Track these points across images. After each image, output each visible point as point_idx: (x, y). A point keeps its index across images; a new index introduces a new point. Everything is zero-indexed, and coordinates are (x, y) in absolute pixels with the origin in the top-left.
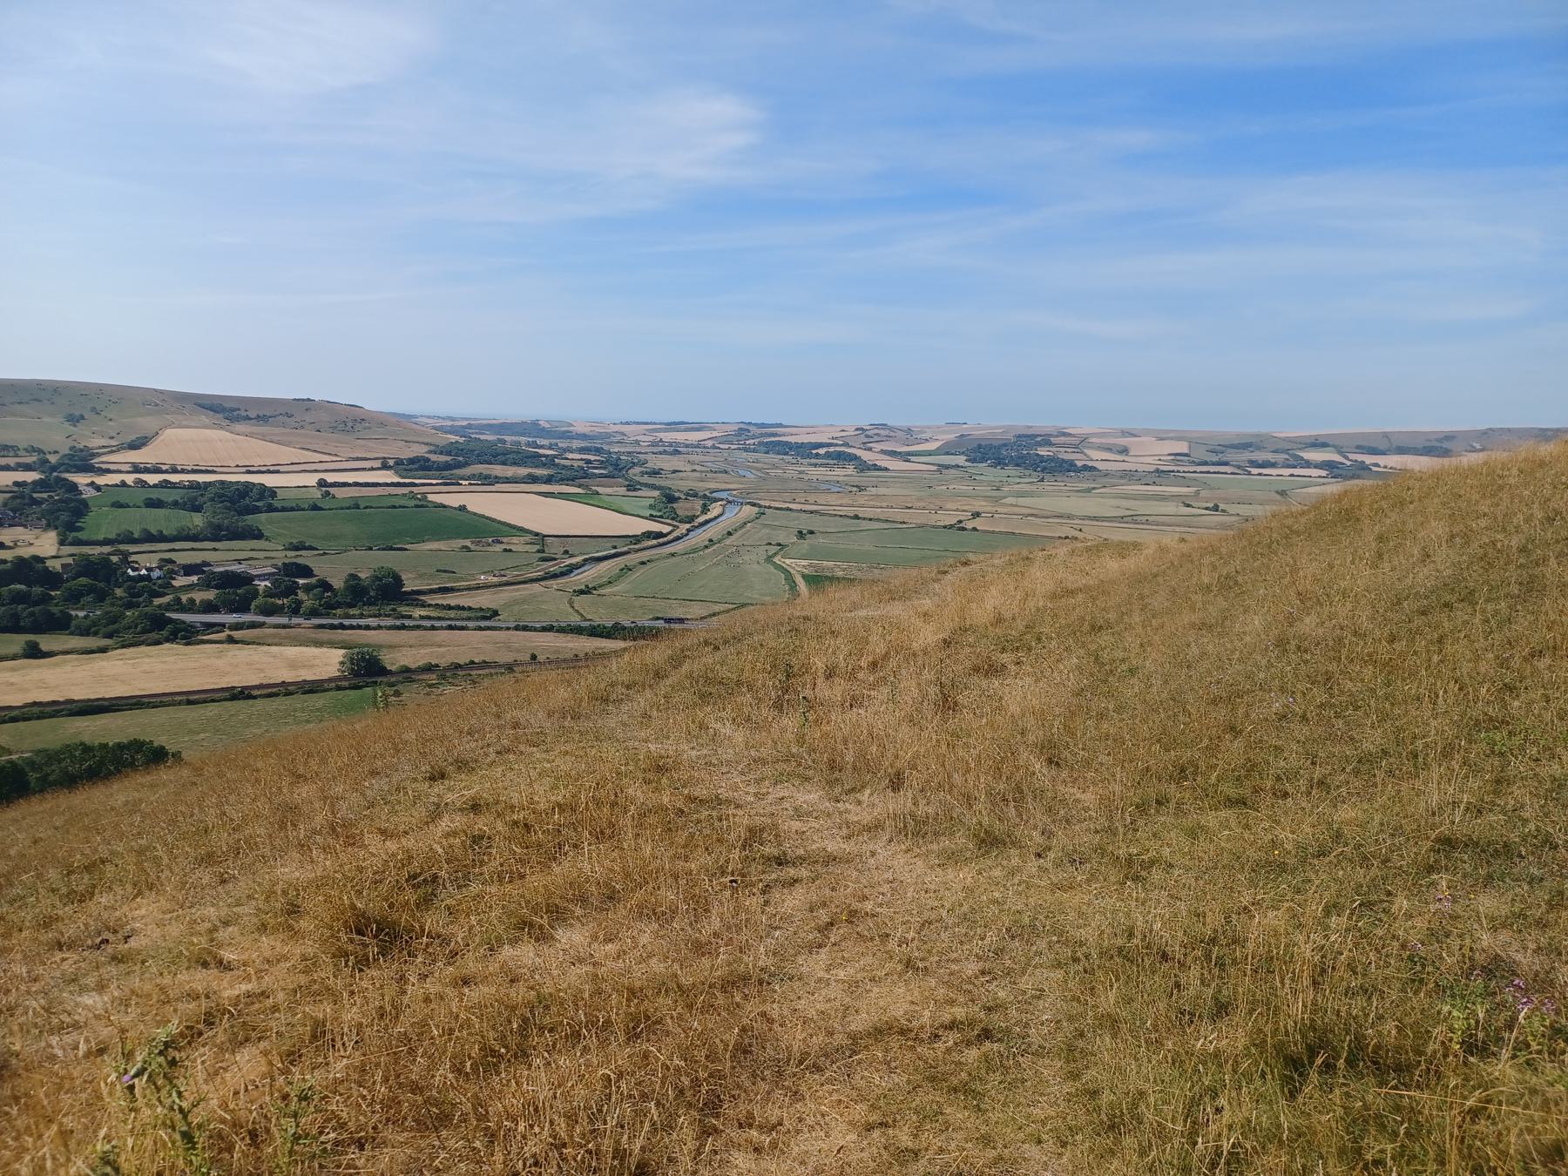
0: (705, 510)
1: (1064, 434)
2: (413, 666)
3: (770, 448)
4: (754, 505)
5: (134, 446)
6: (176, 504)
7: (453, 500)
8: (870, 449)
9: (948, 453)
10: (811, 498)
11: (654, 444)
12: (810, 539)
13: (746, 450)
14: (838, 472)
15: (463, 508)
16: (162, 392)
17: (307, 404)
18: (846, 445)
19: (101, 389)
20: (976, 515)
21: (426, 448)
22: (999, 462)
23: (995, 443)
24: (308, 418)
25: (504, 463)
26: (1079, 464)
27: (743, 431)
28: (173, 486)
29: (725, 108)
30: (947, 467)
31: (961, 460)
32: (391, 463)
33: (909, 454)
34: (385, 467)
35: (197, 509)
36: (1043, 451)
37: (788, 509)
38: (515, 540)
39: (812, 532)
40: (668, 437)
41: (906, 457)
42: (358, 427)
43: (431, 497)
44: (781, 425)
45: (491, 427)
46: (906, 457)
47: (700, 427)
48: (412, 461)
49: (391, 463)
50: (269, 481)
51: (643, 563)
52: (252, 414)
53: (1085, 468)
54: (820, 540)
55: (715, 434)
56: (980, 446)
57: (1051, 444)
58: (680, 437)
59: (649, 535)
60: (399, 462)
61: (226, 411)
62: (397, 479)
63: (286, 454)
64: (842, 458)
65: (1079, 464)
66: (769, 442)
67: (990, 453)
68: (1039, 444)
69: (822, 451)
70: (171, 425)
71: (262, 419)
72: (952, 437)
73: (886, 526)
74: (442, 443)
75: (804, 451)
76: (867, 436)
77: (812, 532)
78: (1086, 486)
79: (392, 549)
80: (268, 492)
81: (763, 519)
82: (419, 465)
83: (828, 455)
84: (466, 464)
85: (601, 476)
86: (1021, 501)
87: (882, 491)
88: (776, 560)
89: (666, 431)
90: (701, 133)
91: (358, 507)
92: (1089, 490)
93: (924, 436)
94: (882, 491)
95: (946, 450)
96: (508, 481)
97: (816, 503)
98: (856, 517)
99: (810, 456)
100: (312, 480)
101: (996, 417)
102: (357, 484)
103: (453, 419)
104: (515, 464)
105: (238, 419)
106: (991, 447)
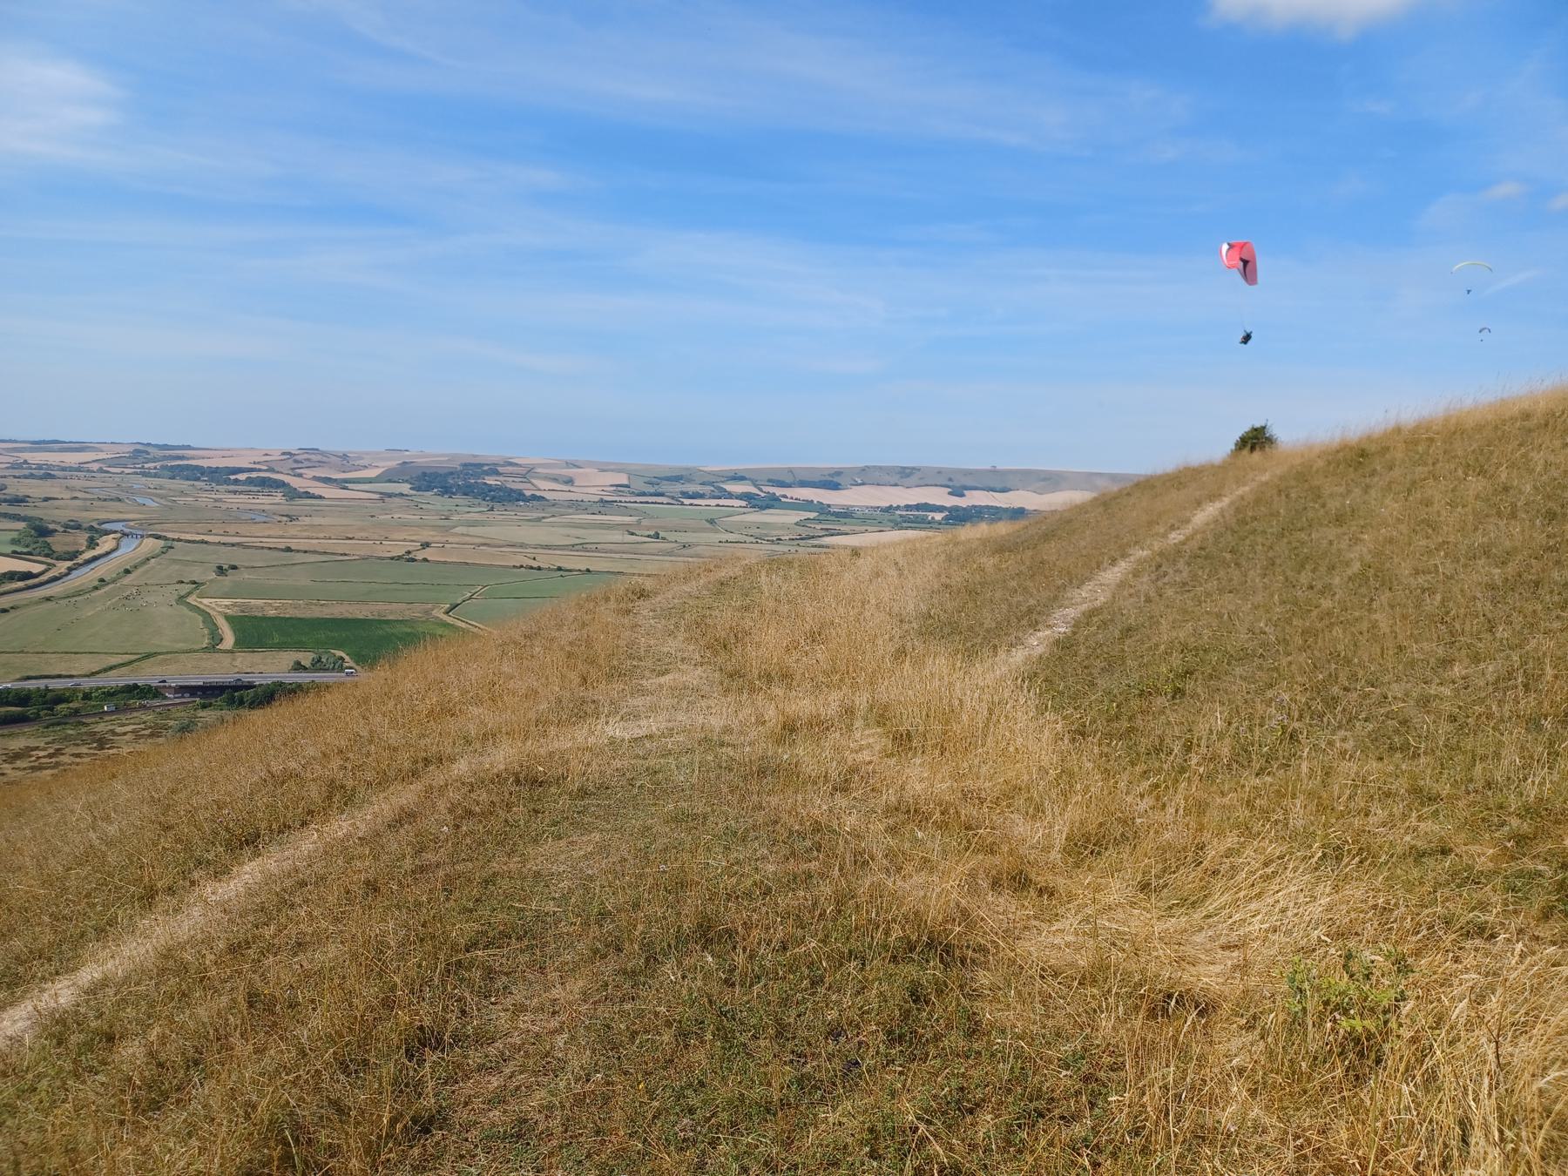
1: (511, 464)
3: (176, 472)
10: (232, 529)
13: (144, 474)
18: (271, 470)
26: (528, 493)
30: (390, 495)
31: (405, 488)
33: (346, 481)
36: (491, 481)
39: (234, 568)
44: (189, 448)
47: (81, 448)
57: (498, 473)
58: (53, 458)
64: (264, 483)
66: (181, 468)
67: (435, 480)
68: (487, 473)
69: (242, 477)
73: (324, 558)
76: (296, 460)
77: (234, 568)
83: (250, 481)
86: (472, 530)
87: (317, 520)
93: (361, 462)
95: (388, 477)
97: (226, 533)
99: (227, 482)
101: (442, 446)
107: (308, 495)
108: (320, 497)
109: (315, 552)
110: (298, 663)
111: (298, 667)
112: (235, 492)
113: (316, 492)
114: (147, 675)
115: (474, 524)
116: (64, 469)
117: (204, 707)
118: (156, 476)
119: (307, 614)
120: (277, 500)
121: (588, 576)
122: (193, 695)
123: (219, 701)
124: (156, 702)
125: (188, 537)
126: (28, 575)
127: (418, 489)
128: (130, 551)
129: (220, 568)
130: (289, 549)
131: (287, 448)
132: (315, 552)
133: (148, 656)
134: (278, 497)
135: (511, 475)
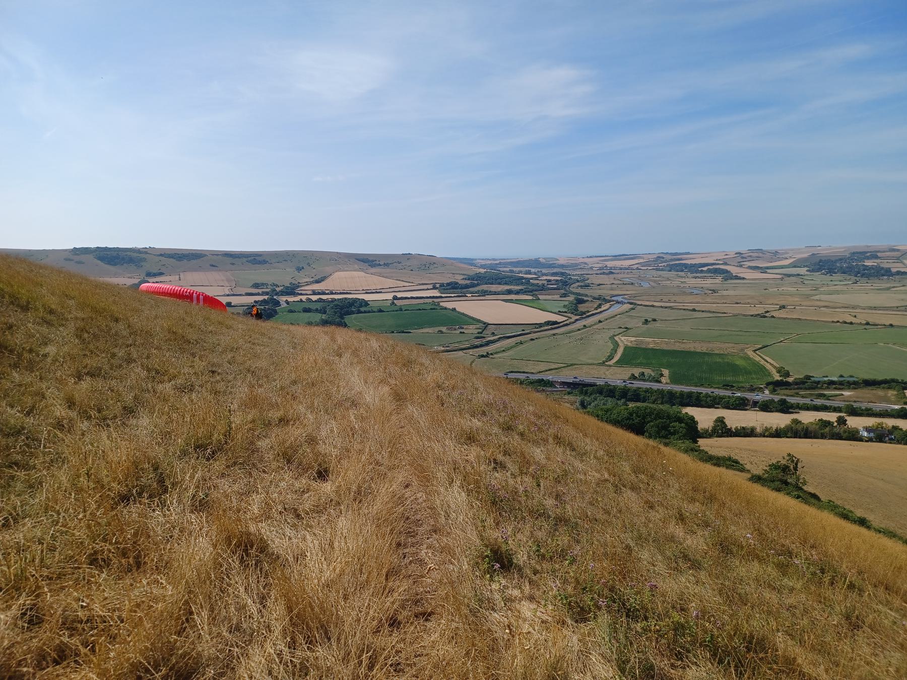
0: (600, 306)
1: (894, 250)
2: (817, 375)
3: (671, 268)
4: (631, 303)
5: (318, 282)
6: (317, 310)
7: (450, 305)
8: (741, 266)
9: (795, 267)
10: (665, 299)
11: (601, 269)
12: (651, 325)
13: (657, 270)
14: (709, 281)
15: (454, 309)
16: (340, 254)
17: (408, 256)
18: (725, 264)
19: (312, 253)
20: (783, 307)
21: (463, 277)
22: (831, 271)
23: (833, 259)
24: (408, 263)
25: (500, 284)
26: (894, 270)
27: (659, 258)
28: (323, 301)
29: (564, 73)
30: (789, 276)
31: (803, 271)
32: (438, 286)
33: (768, 268)
34: (434, 288)
35: (325, 313)
36: (868, 263)
37: (653, 306)
38: (471, 327)
39: (654, 320)
40: (610, 264)
41: (763, 270)
42: (431, 267)
43: (442, 304)
44: (688, 253)
45: (518, 263)
46: (763, 270)
47: (634, 257)
48: (448, 284)
49: (438, 286)
50: (367, 297)
51: (532, 340)
52: (382, 263)
53: (898, 273)
54: (657, 325)
55: (641, 261)
56: (821, 261)
57: (877, 257)
58: (618, 263)
59: (548, 323)
60: (442, 285)
61: (368, 262)
62: (439, 295)
63: (390, 283)
64: (717, 272)
65: (894, 270)
66: (678, 265)
67: (825, 265)
68: (868, 258)
69: (705, 269)
70: (340, 270)
71: (386, 265)
72: (806, 255)
73: (711, 315)
74: (471, 273)
75: (694, 269)
76: (741, 258)
77: (654, 320)
78: (888, 285)
79: (403, 332)
80: (366, 303)
81: (633, 313)
82: (453, 287)
83: (709, 271)
84: (478, 285)
85: (554, 289)
86: (833, 297)
87: (725, 293)
88: (616, 338)
89: (612, 260)
90: (552, 91)
91: (401, 310)
92: (888, 289)
93: (786, 256)
94: (725, 293)
95: (794, 265)
96: (495, 293)
97: (675, 302)
98: (694, 310)
99: (697, 272)
100: (390, 296)
101: (836, 241)
102: (412, 298)
103: (494, 260)
104: (506, 284)
105: (373, 266)
106: (829, 261)
107: (737, 278)
108: (744, 278)
109: (709, 312)
110: (633, 375)
111: (633, 377)
112: (696, 278)
113: (742, 275)
114: (549, 377)
115: (837, 292)
116: (621, 269)
117: (569, 393)
118: (662, 270)
119: (665, 347)
120: (717, 281)
121: (891, 329)
122: (568, 387)
123: (576, 391)
124: (550, 389)
125: (647, 303)
126: (556, 323)
127: (813, 271)
128: (617, 309)
129: (646, 320)
130: (694, 310)
131: (738, 250)
132: (709, 312)
133: (572, 365)
134: (719, 280)
135: (888, 258)
